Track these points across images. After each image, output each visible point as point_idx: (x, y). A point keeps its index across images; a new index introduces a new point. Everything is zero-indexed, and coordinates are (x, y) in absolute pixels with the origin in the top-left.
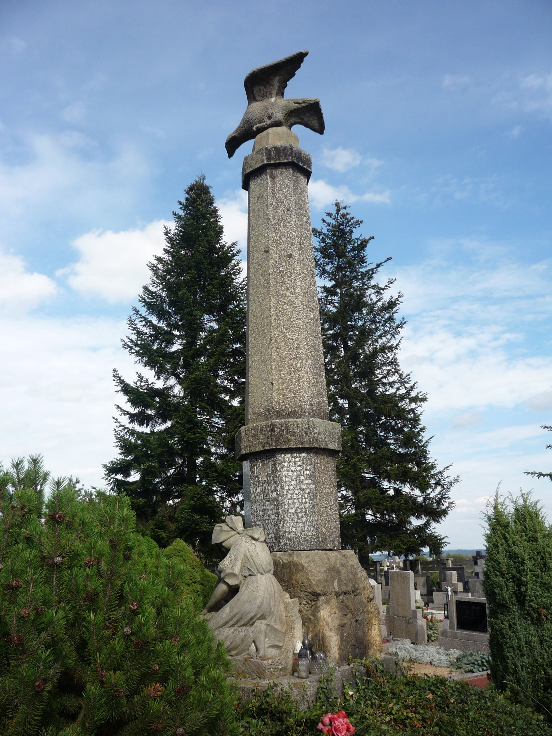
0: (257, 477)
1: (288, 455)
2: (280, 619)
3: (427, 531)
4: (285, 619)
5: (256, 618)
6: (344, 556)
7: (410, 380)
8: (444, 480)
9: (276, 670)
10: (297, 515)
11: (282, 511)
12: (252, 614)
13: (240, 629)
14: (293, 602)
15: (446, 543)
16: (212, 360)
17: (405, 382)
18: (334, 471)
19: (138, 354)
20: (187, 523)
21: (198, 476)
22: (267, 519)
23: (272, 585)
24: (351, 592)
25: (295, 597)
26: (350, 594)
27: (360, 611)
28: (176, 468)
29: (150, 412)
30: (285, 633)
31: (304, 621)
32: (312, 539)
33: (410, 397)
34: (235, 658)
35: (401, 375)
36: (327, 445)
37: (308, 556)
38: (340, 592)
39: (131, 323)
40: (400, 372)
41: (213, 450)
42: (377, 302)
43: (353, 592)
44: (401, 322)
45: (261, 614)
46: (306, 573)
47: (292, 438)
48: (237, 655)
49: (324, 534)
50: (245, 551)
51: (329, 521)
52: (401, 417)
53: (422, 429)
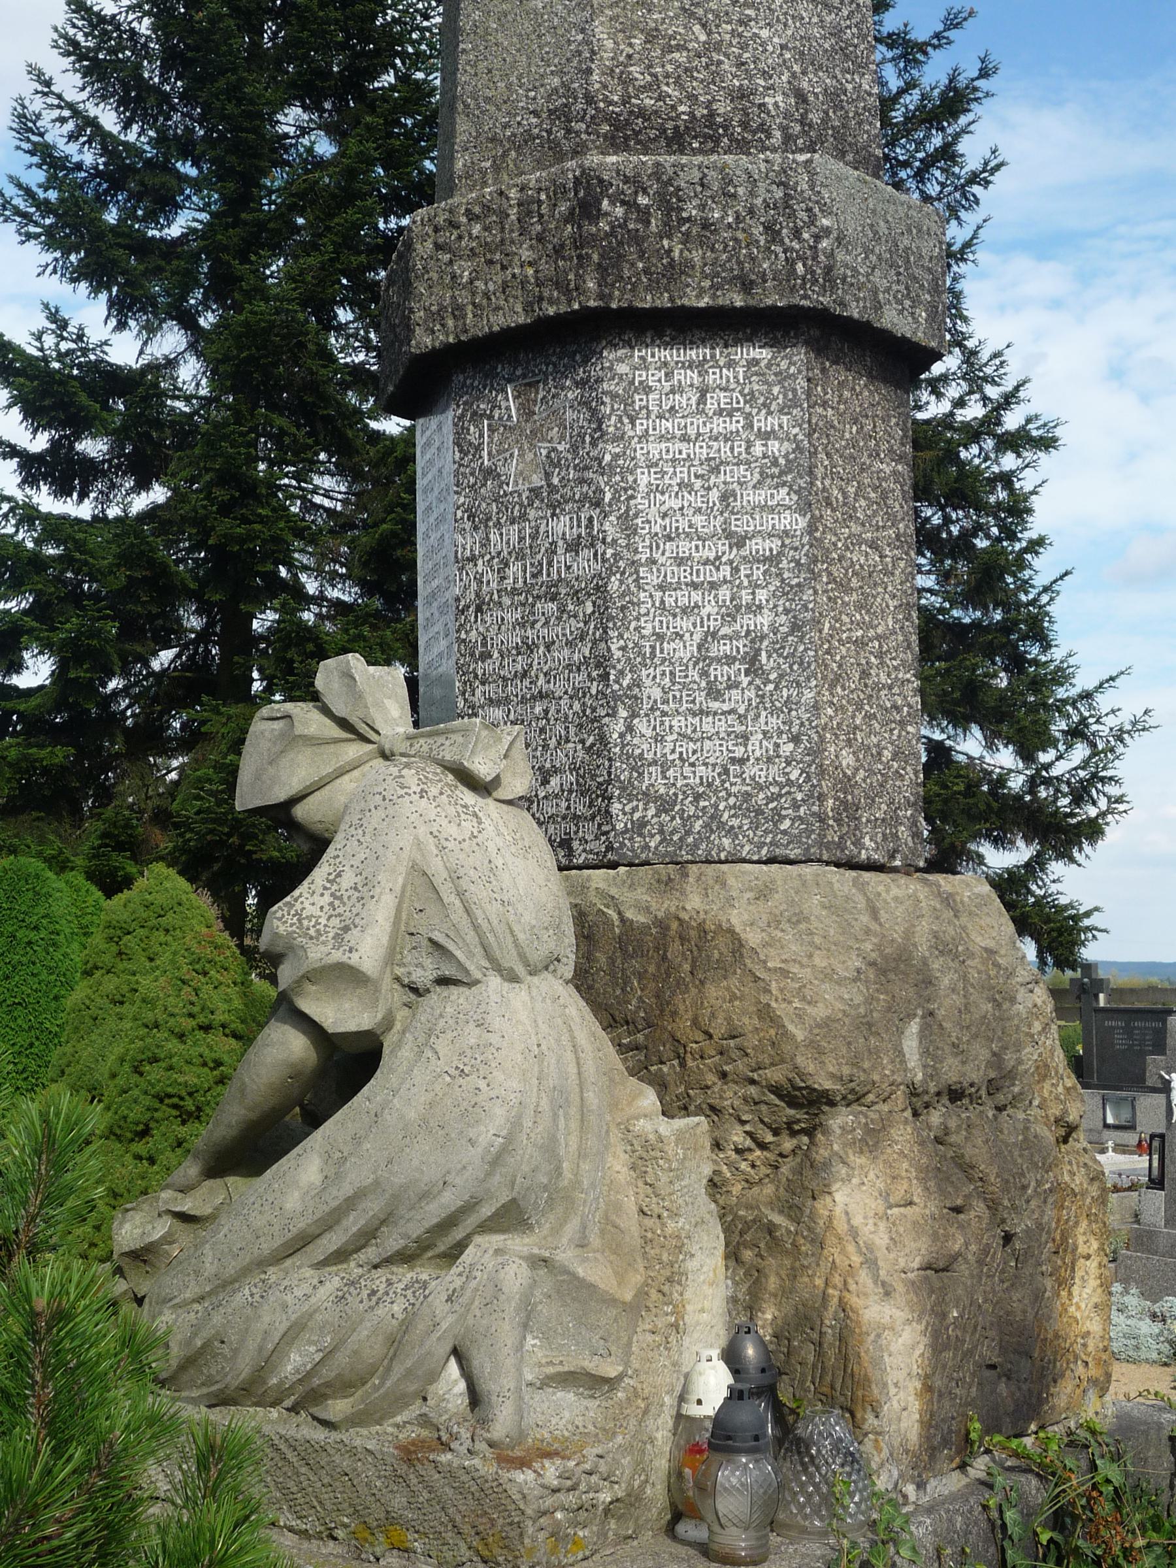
0: (490, 473)
1: (665, 354)
2: (610, 1226)
3: (1034, 887)
4: (635, 1231)
5: (472, 1221)
6: (948, 900)
7: (1002, 371)
8: (1098, 722)
9: (583, 1515)
10: (704, 674)
11: (623, 649)
12: (449, 1200)
13: (379, 1279)
14: (680, 1136)
15: (1096, 929)
16: (313, 260)
17: (985, 379)
18: (900, 459)
19: (51, 240)
20: (211, 831)
21: (255, 675)
22: (542, 696)
23: (565, 1038)
24: (983, 1093)
25: (685, 1110)
26: (975, 1099)
27: (1024, 1188)
28: (184, 647)
29: (93, 447)
30: (636, 1308)
31: (736, 1238)
32: (785, 802)
33: (999, 431)
34: (344, 1436)
35: (970, 356)
36: (878, 307)
37: (763, 893)
38: (933, 1088)
39: (25, 124)
40: (970, 344)
41: (311, 586)
42: (902, 92)
43: (993, 1087)
44: (986, 164)
45: (504, 1197)
46: (757, 979)
47: (696, 256)
48: (356, 1420)
49: (846, 785)
50: (418, 844)
51: (869, 717)
52: (964, 497)
53: (1036, 545)
